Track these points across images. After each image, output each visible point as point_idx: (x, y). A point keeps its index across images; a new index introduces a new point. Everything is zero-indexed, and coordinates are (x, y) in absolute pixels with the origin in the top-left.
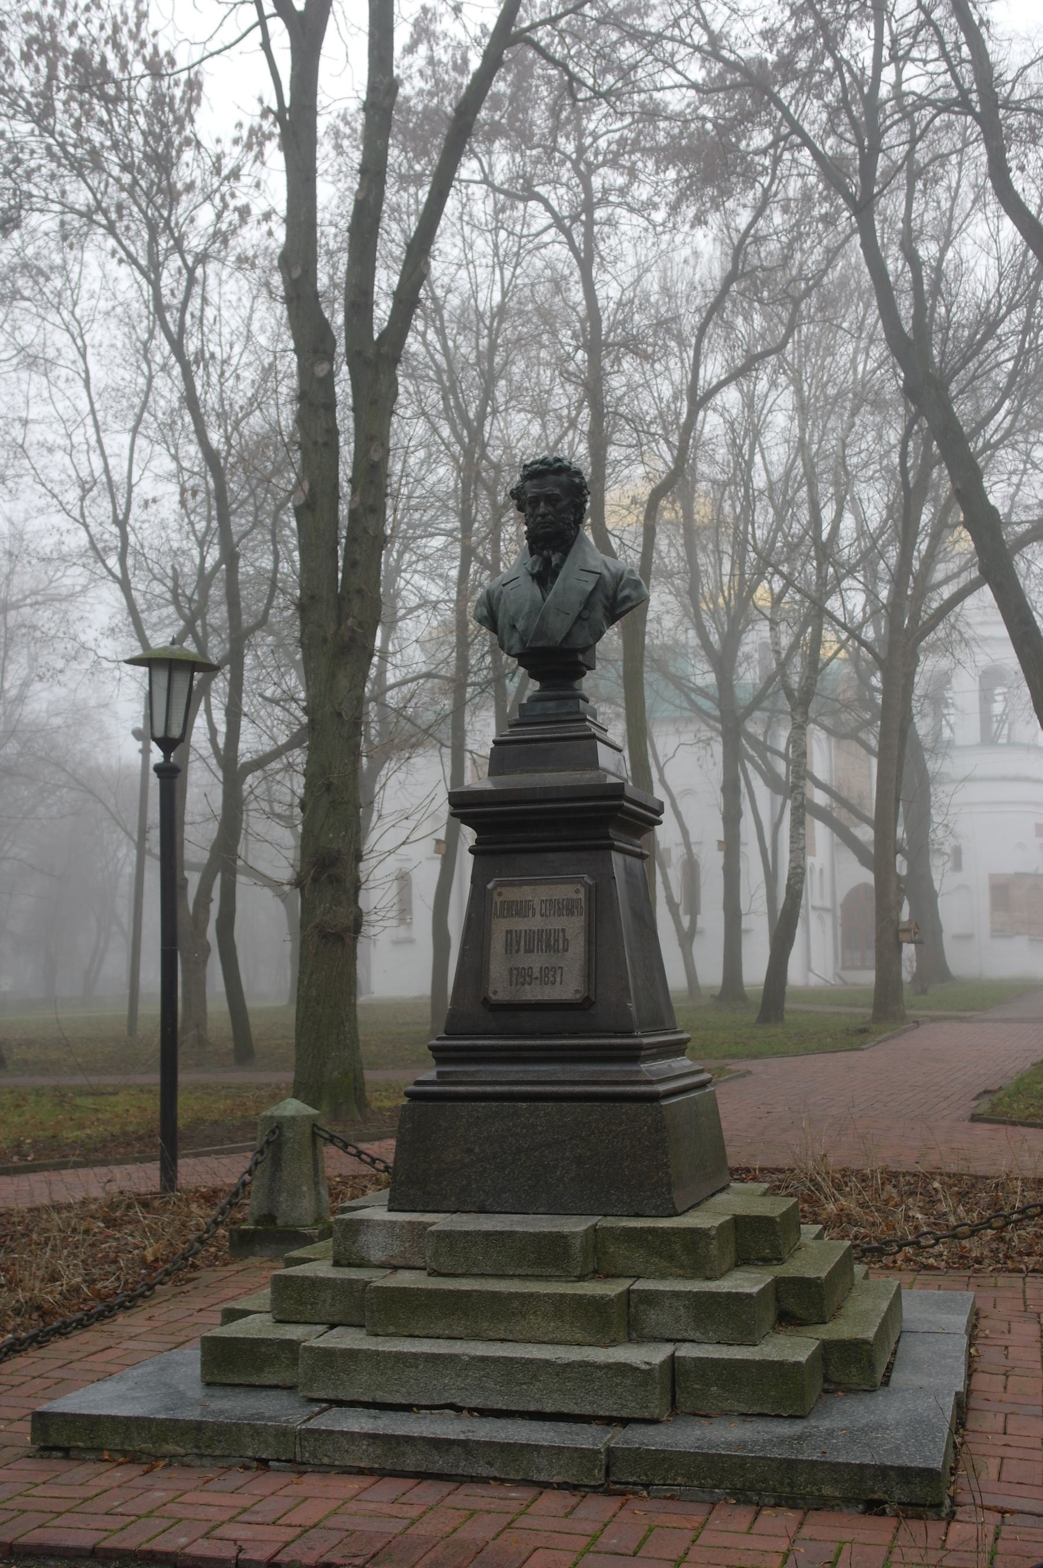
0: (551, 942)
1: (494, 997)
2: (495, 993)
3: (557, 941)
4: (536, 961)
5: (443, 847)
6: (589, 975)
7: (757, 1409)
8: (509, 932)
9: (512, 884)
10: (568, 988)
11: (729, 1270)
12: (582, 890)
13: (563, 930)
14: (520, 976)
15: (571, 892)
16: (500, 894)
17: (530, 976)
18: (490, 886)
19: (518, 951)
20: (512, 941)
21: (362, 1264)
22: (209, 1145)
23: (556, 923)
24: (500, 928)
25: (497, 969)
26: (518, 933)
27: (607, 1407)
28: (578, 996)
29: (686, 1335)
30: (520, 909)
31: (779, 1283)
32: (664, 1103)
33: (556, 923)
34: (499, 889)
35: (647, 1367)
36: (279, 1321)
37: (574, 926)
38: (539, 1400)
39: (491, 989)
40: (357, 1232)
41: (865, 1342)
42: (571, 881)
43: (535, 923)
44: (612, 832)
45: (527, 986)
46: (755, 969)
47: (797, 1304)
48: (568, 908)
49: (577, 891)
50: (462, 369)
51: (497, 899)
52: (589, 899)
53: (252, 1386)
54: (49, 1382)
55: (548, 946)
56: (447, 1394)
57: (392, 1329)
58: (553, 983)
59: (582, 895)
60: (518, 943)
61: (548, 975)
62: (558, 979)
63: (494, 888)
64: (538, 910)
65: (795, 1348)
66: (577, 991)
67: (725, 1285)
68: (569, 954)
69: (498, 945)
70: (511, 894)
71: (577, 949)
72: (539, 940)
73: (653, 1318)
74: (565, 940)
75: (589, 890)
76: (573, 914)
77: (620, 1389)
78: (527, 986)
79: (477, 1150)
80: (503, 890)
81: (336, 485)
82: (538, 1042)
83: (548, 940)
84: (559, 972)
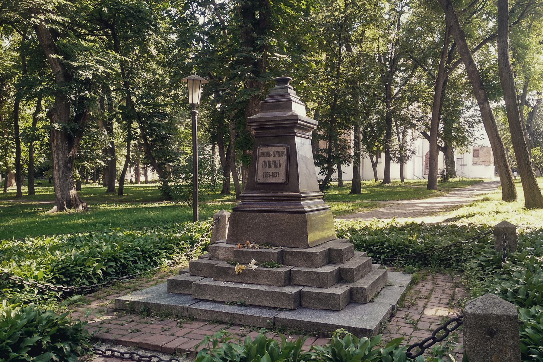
0: (276, 164)
3: (277, 164)
4: (271, 170)
6: (287, 175)
7: (325, 308)
9: (265, 147)
10: (280, 179)
11: (324, 265)
14: (266, 175)
15: (282, 149)
20: (265, 164)
21: (218, 259)
23: (277, 159)
27: (278, 305)
29: (307, 284)
30: (268, 154)
31: (340, 269)
32: (306, 214)
37: (283, 160)
38: (259, 302)
40: (215, 250)
41: (365, 289)
42: (283, 146)
43: (271, 159)
44: (295, 131)
46: (303, 195)
47: (342, 277)
48: (281, 154)
52: (288, 151)
53: (181, 294)
54: (188, 336)
59: (285, 150)
61: (275, 175)
65: (340, 290)
67: (320, 270)
68: (281, 168)
69: (260, 164)
70: (264, 150)
71: (283, 168)
73: (297, 279)
74: (280, 164)
75: (288, 149)
77: (282, 300)
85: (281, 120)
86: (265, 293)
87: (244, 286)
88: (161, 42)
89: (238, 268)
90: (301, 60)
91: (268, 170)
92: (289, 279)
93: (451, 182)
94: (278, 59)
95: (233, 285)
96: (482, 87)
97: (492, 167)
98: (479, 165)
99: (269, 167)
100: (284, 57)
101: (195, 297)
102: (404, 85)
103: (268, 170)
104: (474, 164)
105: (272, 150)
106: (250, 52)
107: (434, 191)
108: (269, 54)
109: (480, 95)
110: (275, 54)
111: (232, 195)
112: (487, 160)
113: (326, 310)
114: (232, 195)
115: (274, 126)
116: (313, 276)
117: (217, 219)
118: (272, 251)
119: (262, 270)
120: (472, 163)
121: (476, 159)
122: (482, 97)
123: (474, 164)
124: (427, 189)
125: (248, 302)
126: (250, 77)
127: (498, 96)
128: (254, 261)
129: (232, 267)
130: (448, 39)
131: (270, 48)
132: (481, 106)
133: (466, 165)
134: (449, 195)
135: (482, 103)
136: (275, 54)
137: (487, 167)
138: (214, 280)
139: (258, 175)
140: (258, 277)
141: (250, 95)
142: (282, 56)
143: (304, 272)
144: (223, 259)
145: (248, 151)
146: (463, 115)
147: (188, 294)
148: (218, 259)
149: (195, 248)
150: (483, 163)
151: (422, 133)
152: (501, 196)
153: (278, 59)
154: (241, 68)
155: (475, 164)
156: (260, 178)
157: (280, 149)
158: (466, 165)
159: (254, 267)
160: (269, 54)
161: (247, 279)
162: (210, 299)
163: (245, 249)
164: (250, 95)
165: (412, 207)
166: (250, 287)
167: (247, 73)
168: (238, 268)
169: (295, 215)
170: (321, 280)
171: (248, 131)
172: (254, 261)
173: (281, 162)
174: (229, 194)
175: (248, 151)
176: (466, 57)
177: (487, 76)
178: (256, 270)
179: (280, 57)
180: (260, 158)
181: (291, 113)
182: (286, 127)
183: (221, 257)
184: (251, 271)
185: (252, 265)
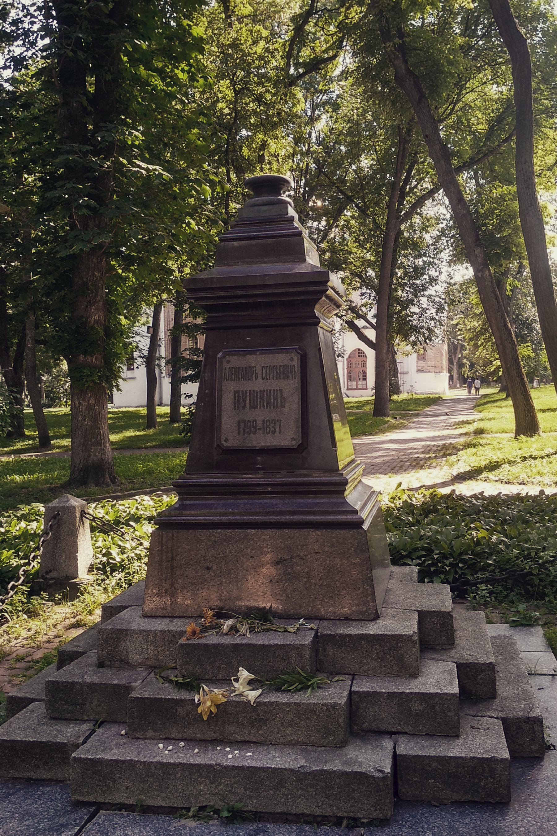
1: (225, 444)
2: (226, 440)
4: (260, 415)
7: (469, 797)
9: (237, 353)
10: (287, 437)
12: (296, 359)
13: (281, 391)
14: (247, 428)
16: (228, 362)
17: (255, 428)
18: (220, 355)
19: (244, 407)
20: (240, 400)
21: (124, 664)
22: (274, 346)
23: (273, 385)
25: (228, 421)
26: (244, 393)
30: (247, 373)
33: (273, 385)
34: (228, 358)
35: (381, 775)
36: (52, 718)
37: (290, 387)
39: (223, 438)
42: (287, 351)
43: (257, 385)
48: (284, 373)
53: (29, 779)
56: (202, 799)
57: (150, 733)
58: (274, 433)
60: (244, 401)
61: (269, 427)
62: (277, 429)
63: (224, 357)
68: (286, 410)
69: (227, 400)
70: (236, 361)
71: (293, 407)
72: (262, 399)
74: (282, 397)
78: (252, 435)
79: (215, 568)
81: (144, 435)
84: (278, 423)
85: (254, 287)
86: (301, 776)
87: (231, 757)
89: (209, 697)
90: (187, 177)
91: (249, 415)
92: (357, 722)
93: (397, 402)
94: (144, 172)
95: (196, 756)
96: (478, 242)
97: (445, 375)
98: (426, 372)
100: (155, 170)
101: (81, 798)
102: (322, 242)
103: (249, 415)
104: (418, 371)
105: (258, 361)
106: (86, 154)
107: (387, 419)
108: (125, 162)
109: (476, 256)
110: (137, 162)
111: (30, 438)
112: (437, 364)
113: (473, 803)
114: (30, 438)
116: (417, 706)
117: (54, 517)
118: (290, 640)
119: (277, 704)
120: (416, 369)
121: (422, 363)
122: (480, 260)
123: (418, 371)
124: (374, 415)
125: (251, 805)
126: (88, 207)
127: (504, 259)
128: (244, 674)
129: (184, 695)
130: (401, 163)
131: (125, 149)
132: (480, 274)
133: (407, 373)
134: (412, 425)
135: (481, 271)
136: (137, 162)
137: (437, 375)
138: (132, 736)
140: (265, 722)
141: (89, 242)
142: (151, 167)
143: (392, 695)
144: (140, 665)
145: (82, 357)
146: (426, 293)
147: (51, 780)
148: (124, 664)
149: (12, 593)
150: (432, 369)
151: (347, 322)
152: (512, 425)
153: (144, 172)
154: (69, 186)
157: (281, 359)
158: (407, 373)
159: (252, 695)
160: (125, 162)
161: (232, 729)
162: (131, 801)
163: (212, 639)
164: (89, 242)
166: (250, 758)
167: (81, 198)
168: (209, 697)
169: (336, 532)
170: (440, 717)
171: (82, 317)
172: (244, 674)
173: (285, 393)
174: (23, 437)
175: (82, 357)
176: (453, 189)
177: (485, 225)
178: (258, 704)
179: (147, 170)
180: (225, 384)
181: (303, 265)
183: (135, 658)
184: (244, 706)
185: (244, 687)
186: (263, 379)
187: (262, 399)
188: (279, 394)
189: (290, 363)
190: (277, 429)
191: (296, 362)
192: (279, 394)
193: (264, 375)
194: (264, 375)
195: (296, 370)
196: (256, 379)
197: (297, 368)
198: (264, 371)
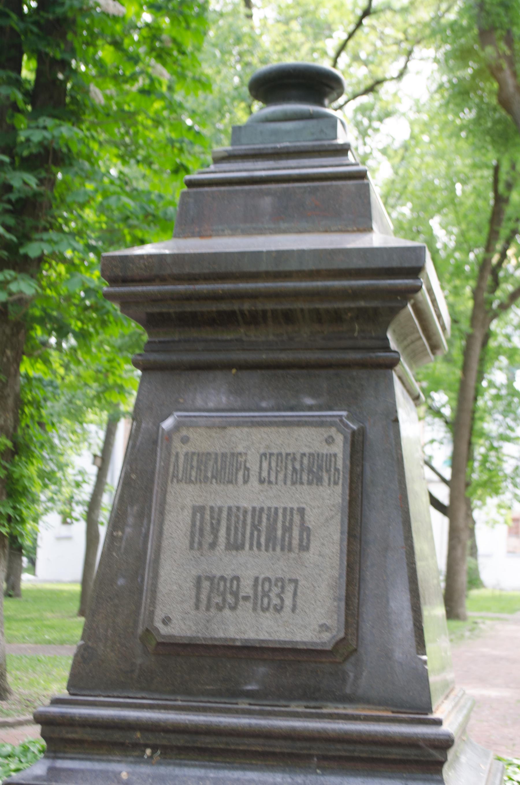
0: (279, 532)
1: (164, 630)
2: (166, 621)
3: (288, 529)
4: (249, 566)
5: (99, 461)
8: (198, 510)
10: (309, 619)
12: (339, 439)
13: (302, 511)
15: (319, 438)
17: (235, 594)
18: (168, 424)
19: (213, 545)
20: (205, 529)
23: (284, 497)
24: (181, 503)
26: (216, 513)
28: (326, 637)
30: (226, 468)
33: (284, 497)
37: (324, 505)
39: (159, 614)
43: (248, 495)
45: (227, 612)
48: (313, 470)
49: (330, 441)
50: (34, 708)
51: (180, 449)
55: (271, 539)
58: (279, 609)
60: (215, 531)
61: (266, 595)
62: (288, 602)
63: (177, 427)
64: (254, 468)
66: (324, 628)
68: (310, 557)
69: (176, 526)
70: (202, 441)
72: (255, 527)
74: (305, 529)
76: (319, 480)
78: (227, 612)
80: (191, 434)
82: (244, 721)
83: (272, 529)
84: (290, 588)
88: (101, 288)
99: (234, 546)
104: (509, 552)
105: (251, 442)
115: (270, 306)
123: (509, 552)
139: (163, 588)
155: (511, 552)
156: (177, 611)
165: (187, 470)
173: (311, 519)
182: (337, 317)
186: (261, 481)
187: (255, 527)
188: (297, 518)
189: (325, 450)
190: (288, 602)
191: (339, 448)
192: (297, 518)
193: (265, 474)
194: (265, 474)
195: (340, 464)
196: (246, 482)
197: (341, 462)
198: (265, 465)
